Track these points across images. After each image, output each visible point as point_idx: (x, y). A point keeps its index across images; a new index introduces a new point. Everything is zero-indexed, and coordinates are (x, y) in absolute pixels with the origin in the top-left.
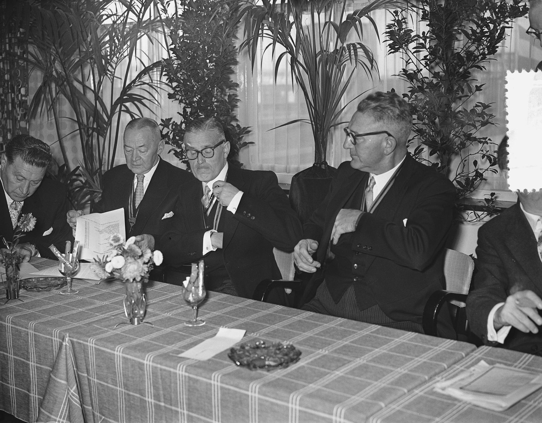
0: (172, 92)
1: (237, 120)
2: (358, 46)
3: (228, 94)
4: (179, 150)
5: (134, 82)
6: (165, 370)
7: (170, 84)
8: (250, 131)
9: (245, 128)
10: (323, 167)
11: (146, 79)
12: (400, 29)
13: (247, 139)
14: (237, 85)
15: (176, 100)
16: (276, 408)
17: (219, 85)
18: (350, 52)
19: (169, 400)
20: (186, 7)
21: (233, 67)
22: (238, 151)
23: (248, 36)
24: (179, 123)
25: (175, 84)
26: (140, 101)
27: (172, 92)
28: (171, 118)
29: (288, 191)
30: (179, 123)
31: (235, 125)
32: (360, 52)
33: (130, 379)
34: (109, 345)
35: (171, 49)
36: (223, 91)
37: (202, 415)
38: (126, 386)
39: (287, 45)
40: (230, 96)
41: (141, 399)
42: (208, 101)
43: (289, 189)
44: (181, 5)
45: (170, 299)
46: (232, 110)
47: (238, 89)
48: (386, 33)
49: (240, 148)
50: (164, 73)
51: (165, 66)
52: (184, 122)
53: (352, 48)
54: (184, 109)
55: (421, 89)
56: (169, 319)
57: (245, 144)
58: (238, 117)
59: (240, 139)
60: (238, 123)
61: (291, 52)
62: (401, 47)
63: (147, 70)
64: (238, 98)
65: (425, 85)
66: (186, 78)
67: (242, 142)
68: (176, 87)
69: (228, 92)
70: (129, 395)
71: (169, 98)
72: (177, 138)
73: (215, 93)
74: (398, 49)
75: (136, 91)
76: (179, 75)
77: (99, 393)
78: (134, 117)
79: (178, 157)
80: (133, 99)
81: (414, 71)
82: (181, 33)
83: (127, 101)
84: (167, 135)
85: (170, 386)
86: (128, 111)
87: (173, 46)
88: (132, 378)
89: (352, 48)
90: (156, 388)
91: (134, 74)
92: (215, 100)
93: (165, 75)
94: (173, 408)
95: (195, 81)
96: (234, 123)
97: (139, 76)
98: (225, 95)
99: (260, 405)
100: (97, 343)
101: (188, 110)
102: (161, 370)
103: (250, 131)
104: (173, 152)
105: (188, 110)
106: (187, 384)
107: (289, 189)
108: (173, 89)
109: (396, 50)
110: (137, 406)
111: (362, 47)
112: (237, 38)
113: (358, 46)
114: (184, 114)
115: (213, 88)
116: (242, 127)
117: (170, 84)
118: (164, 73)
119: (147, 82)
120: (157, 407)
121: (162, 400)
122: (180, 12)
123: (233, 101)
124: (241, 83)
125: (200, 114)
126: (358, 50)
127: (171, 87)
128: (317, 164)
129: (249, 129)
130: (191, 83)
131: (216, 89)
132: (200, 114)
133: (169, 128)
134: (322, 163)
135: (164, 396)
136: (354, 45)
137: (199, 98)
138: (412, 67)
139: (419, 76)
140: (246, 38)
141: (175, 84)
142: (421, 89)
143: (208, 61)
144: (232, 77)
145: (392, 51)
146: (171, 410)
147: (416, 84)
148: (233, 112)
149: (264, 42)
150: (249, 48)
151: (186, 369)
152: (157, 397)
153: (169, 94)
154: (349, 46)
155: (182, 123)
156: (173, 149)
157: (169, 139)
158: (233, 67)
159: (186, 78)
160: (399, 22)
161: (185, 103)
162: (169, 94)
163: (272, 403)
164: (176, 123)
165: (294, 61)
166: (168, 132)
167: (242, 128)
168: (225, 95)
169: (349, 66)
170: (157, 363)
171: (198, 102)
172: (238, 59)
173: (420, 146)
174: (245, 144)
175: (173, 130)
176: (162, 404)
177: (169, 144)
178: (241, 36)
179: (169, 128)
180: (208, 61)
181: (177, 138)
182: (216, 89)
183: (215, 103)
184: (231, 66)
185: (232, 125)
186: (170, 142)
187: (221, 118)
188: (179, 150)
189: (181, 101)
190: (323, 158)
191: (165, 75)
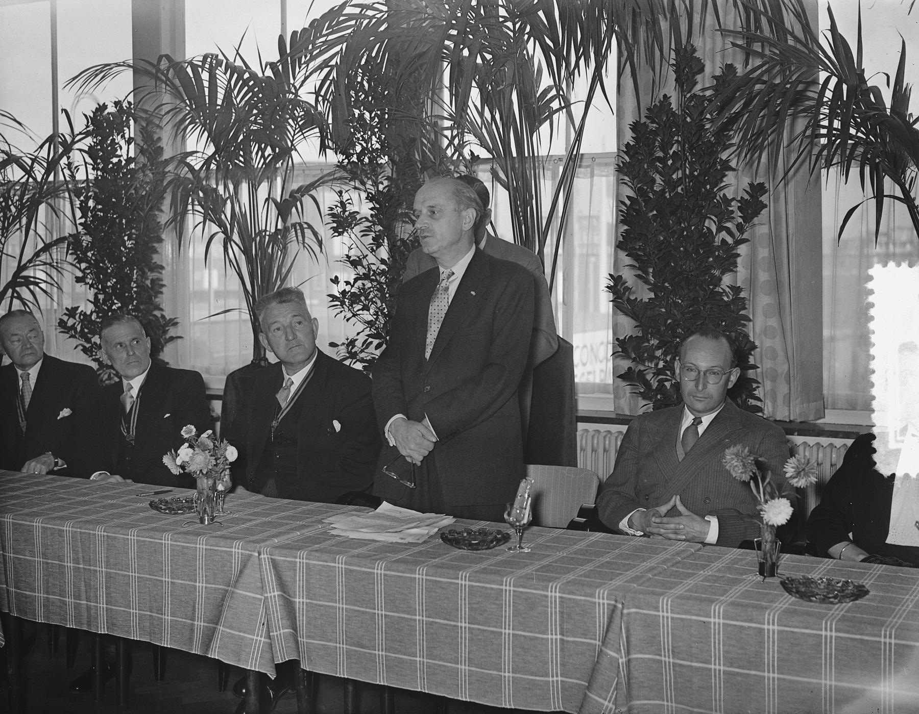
0: (80, 274)
1: (162, 310)
2: (305, 226)
3: (151, 278)
4: (88, 345)
5: (30, 261)
6: (84, 533)
7: (78, 265)
8: (177, 323)
9: (171, 320)
10: (263, 363)
11: (44, 257)
12: (344, 211)
13: (172, 332)
14: (162, 268)
15: (86, 284)
16: (186, 551)
17: (140, 267)
18: (296, 231)
19: (88, 561)
20: (99, 173)
21: (156, 245)
22: (163, 347)
23: (176, 211)
24: (88, 313)
25: (83, 266)
26: (37, 284)
27: (80, 274)
28: (78, 307)
29: (221, 396)
30: (88, 313)
31: (159, 316)
32: (308, 232)
33: (49, 547)
34: (27, 518)
35: (81, 224)
36: (143, 275)
37: (119, 570)
38: (45, 555)
39: (221, 224)
40: (152, 281)
41: (60, 565)
42: (126, 286)
43: (222, 393)
44: (93, 169)
45: (86, 488)
46: (156, 297)
47: (163, 272)
48: (329, 215)
49: (166, 343)
50: (70, 252)
51: (72, 243)
52: (95, 311)
53: (298, 228)
54: (96, 295)
55: (366, 277)
56: (85, 501)
57: (172, 339)
58: (163, 306)
59: (165, 332)
60: (164, 313)
61: (225, 232)
62: (344, 230)
63: (47, 248)
64: (164, 283)
65: (372, 273)
66: (98, 258)
67: (168, 336)
68: (86, 269)
69: (151, 275)
70: (47, 563)
71: (77, 282)
72: (86, 330)
73: (135, 276)
74: (343, 232)
75: (29, 273)
76: (89, 254)
77: (14, 567)
78: (762, 32)
79: (87, 354)
80: (27, 282)
81: (358, 257)
82: (91, 203)
83: (21, 285)
84: (73, 327)
85: (89, 548)
86: (19, 298)
87: (83, 220)
88: (52, 546)
89: (298, 228)
90: (75, 552)
91: (28, 253)
92: (135, 285)
93: (71, 254)
94: (92, 568)
95: (109, 262)
96: (157, 313)
97: (37, 254)
98: (147, 279)
99: (172, 550)
100: (14, 517)
101: (101, 297)
102: (81, 533)
103: (177, 323)
104: (81, 348)
105: (101, 297)
106: (106, 543)
107: (222, 393)
108: (83, 271)
109: (340, 234)
110: (56, 573)
111: (310, 227)
112: (162, 211)
113: (305, 226)
114: (96, 302)
115: (132, 270)
116: (168, 318)
117: (78, 265)
118: (70, 252)
119: (48, 261)
120: (76, 569)
121: (81, 562)
122: (91, 177)
123: (157, 286)
124: (168, 265)
125: (116, 301)
126: (306, 230)
127: (80, 269)
128: (256, 360)
129: (175, 321)
130: (105, 265)
131: (135, 271)
132: (116, 301)
133: (75, 319)
134: (261, 359)
135: (84, 558)
136: (300, 224)
137: (115, 283)
138: (354, 253)
139: (365, 263)
140: (172, 215)
141: (83, 266)
142: (366, 277)
143: (126, 238)
144: (156, 258)
145: (336, 234)
146: (90, 570)
147: (361, 271)
148: (157, 300)
149: (194, 219)
150: (176, 225)
151: (105, 529)
152: (76, 561)
153: (76, 277)
154: (294, 225)
155: (92, 313)
156: (81, 344)
157: (76, 331)
158: (156, 245)
159: (98, 258)
160: (343, 205)
161: (97, 288)
162: (76, 277)
163: (183, 547)
164: (85, 313)
165: (228, 240)
166: (75, 324)
167: (168, 318)
168: (147, 279)
169: (293, 247)
170: (77, 528)
171: (113, 287)
172: (163, 236)
173: (367, 339)
174: (172, 339)
175: (81, 321)
176: (81, 566)
177: (76, 338)
178: (165, 216)
179: (75, 319)
180: (126, 238)
181: (86, 330)
182: (135, 271)
183: (135, 289)
184: (154, 245)
185: (155, 316)
186: (77, 336)
187: (142, 307)
188: (88, 345)
189: (91, 286)
190: (263, 353)
191: (71, 254)
